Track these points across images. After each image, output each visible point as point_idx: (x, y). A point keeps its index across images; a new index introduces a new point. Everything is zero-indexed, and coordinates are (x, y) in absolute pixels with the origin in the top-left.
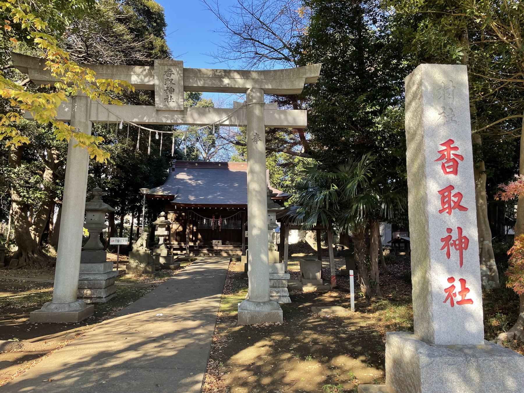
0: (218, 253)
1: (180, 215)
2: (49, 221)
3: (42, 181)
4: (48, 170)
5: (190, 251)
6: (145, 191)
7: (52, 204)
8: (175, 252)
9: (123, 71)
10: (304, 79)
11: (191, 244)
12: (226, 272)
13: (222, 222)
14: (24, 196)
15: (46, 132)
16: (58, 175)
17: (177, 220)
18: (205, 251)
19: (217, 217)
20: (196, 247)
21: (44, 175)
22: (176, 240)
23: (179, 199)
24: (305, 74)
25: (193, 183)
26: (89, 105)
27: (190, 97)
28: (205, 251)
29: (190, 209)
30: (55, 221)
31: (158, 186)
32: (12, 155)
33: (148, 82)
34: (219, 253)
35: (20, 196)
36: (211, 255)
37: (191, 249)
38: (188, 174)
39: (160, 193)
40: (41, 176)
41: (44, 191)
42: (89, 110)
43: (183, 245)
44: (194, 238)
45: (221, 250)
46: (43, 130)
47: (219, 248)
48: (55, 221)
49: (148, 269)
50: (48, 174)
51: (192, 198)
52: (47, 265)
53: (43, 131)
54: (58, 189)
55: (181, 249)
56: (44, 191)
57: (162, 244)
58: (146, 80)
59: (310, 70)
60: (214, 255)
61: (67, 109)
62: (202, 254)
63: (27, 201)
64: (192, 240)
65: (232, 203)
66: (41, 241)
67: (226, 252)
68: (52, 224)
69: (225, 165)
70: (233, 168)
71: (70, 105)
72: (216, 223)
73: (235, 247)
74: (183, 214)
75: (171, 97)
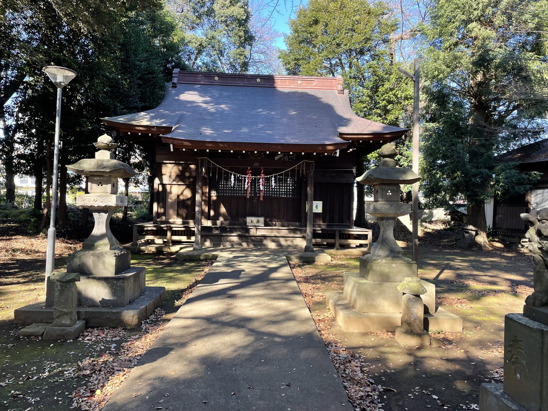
0: (258, 243)
1: (186, 168)
5: (204, 238)
8: (175, 238)
13: (268, 185)
17: (181, 177)
18: (234, 238)
19: (256, 173)
20: (217, 228)
22: (178, 215)
23: (181, 133)
25: (211, 108)
28: (234, 238)
29: (202, 153)
34: (261, 241)
36: (245, 245)
37: (206, 232)
38: (202, 93)
44: (212, 213)
45: (265, 237)
47: (261, 233)
51: (208, 131)
55: (189, 233)
60: (252, 246)
62: (228, 245)
64: (208, 217)
67: (275, 239)
69: (269, 80)
72: (254, 183)
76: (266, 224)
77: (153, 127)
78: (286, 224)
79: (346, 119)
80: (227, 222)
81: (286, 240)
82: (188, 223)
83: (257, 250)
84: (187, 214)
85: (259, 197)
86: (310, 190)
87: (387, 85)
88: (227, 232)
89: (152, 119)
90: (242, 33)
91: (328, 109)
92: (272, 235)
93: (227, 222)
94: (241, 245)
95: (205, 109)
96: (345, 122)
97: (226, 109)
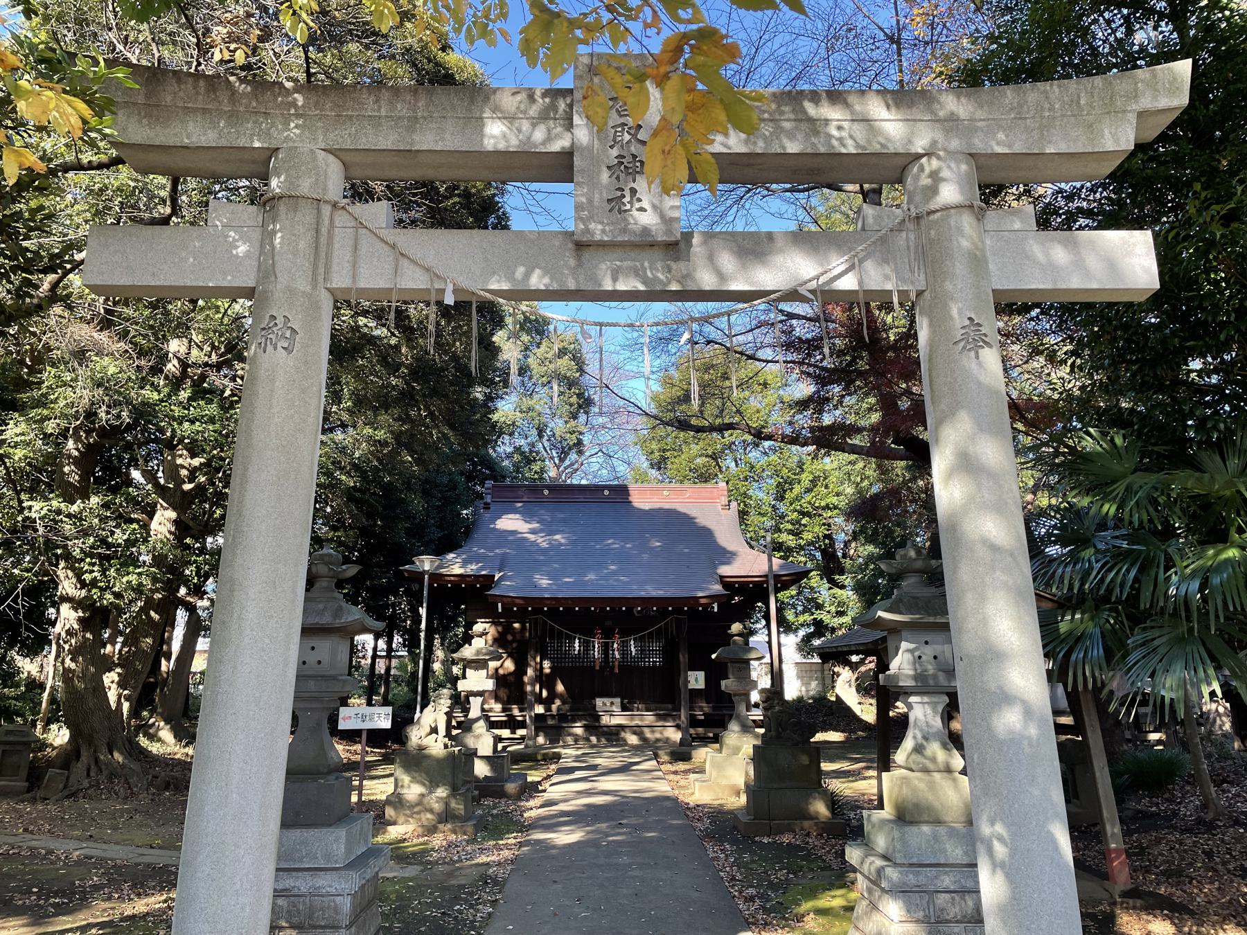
0: (613, 736)
1: (507, 629)
2: (160, 650)
3: (146, 541)
4: (166, 509)
5: (538, 730)
6: (426, 563)
7: (168, 606)
9: (453, 108)
10: (1132, 118)
11: (540, 709)
12: (670, 805)
14: (94, 583)
15: (162, 401)
16: (191, 524)
19: (608, 634)
20: (553, 716)
21: (154, 525)
23: (508, 586)
24: (1135, 96)
25: (542, 541)
26: (324, 230)
27: (522, 328)
30: (176, 646)
31: (451, 551)
32: (66, 469)
33: (544, 143)
34: (618, 734)
35: (83, 584)
36: (594, 739)
38: (527, 516)
39: (457, 570)
40: (146, 527)
41: (151, 566)
42: (323, 249)
43: (516, 712)
44: (545, 694)
45: (622, 727)
46: (155, 393)
47: (616, 721)
48: (176, 646)
49: (453, 804)
50: (163, 522)
51: (544, 582)
52: (150, 784)
53: (156, 396)
54: (189, 563)
56: (151, 566)
57: (477, 719)
58: (539, 134)
59: (1153, 85)
61: (242, 249)
62: (570, 740)
63: (101, 598)
64: (539, 700)
65: (655, 593)
66: (135, 713)
68: (168, 656)
69: (621, 492)
70: (642, 499)
71: (256, 235)
72: (606, 648)
73: (660, 717)
74: (516, 625)
75: (633, 191)
76: (624, 708)
77: (470, 576)
78: (653, 706)
79: (730, 552)
80: (567, 707)
81: (653, 732)
82: (510, 710)
83: (613, 746)
84: (509, 697)
85: (613, 667)
86: (683, 658)
87: (797, 489)
88: (567, 721)
89: (465, 563)
90: (574, 399)
91: (706, 535)
92: (633, 723)
93: (567, 707)
94: (588, 740)
95: (534, 543)
96: (727, 556)
97: (563, 541)
